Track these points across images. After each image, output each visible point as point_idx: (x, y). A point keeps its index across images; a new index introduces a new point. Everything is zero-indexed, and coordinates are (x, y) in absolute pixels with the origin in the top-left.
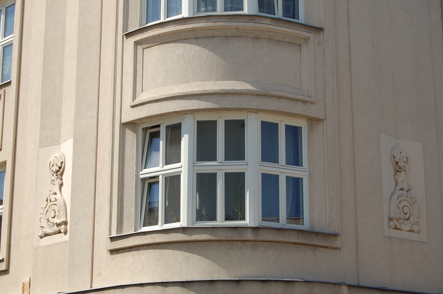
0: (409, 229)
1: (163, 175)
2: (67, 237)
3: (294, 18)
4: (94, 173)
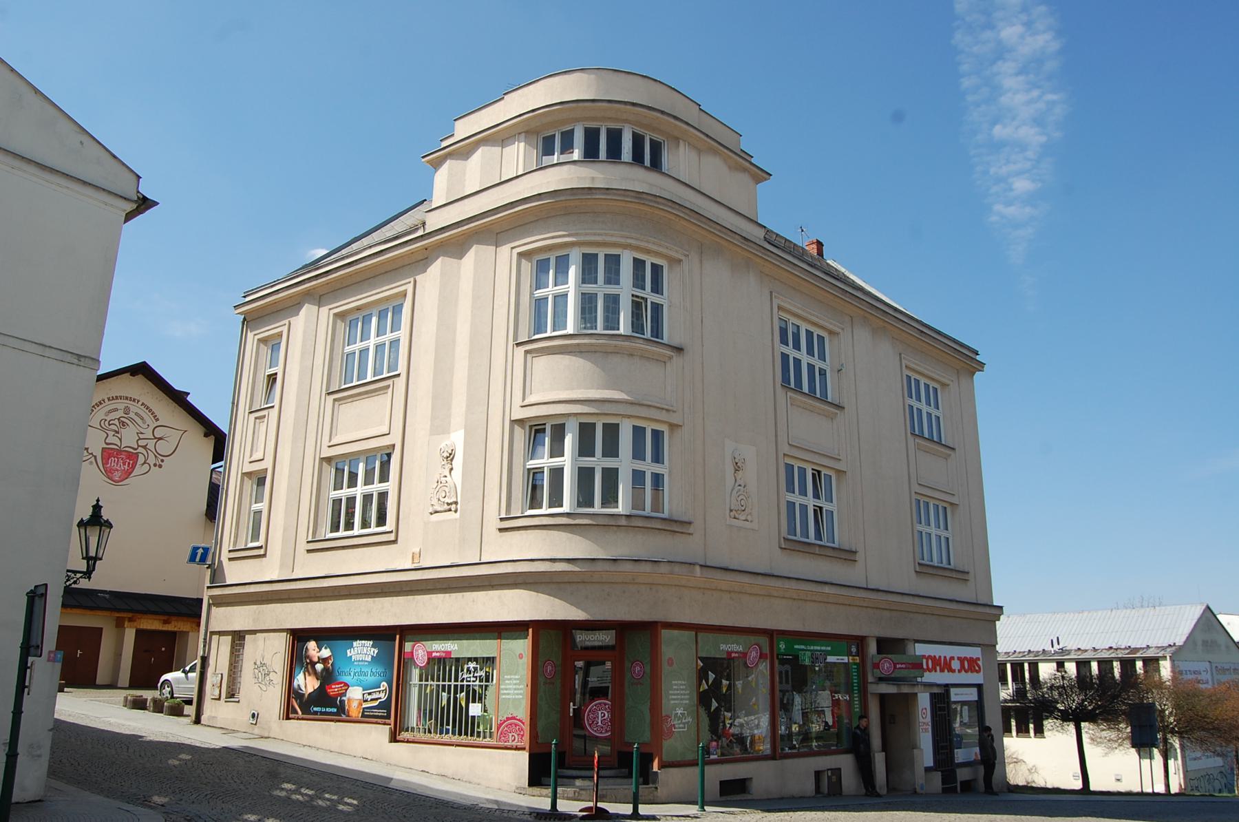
0: (744, 519)
1: (548, 467)
2: (457, 515)
3: (657, 338)
4: (484, 461)
